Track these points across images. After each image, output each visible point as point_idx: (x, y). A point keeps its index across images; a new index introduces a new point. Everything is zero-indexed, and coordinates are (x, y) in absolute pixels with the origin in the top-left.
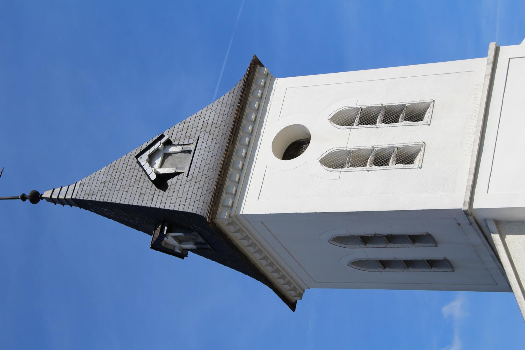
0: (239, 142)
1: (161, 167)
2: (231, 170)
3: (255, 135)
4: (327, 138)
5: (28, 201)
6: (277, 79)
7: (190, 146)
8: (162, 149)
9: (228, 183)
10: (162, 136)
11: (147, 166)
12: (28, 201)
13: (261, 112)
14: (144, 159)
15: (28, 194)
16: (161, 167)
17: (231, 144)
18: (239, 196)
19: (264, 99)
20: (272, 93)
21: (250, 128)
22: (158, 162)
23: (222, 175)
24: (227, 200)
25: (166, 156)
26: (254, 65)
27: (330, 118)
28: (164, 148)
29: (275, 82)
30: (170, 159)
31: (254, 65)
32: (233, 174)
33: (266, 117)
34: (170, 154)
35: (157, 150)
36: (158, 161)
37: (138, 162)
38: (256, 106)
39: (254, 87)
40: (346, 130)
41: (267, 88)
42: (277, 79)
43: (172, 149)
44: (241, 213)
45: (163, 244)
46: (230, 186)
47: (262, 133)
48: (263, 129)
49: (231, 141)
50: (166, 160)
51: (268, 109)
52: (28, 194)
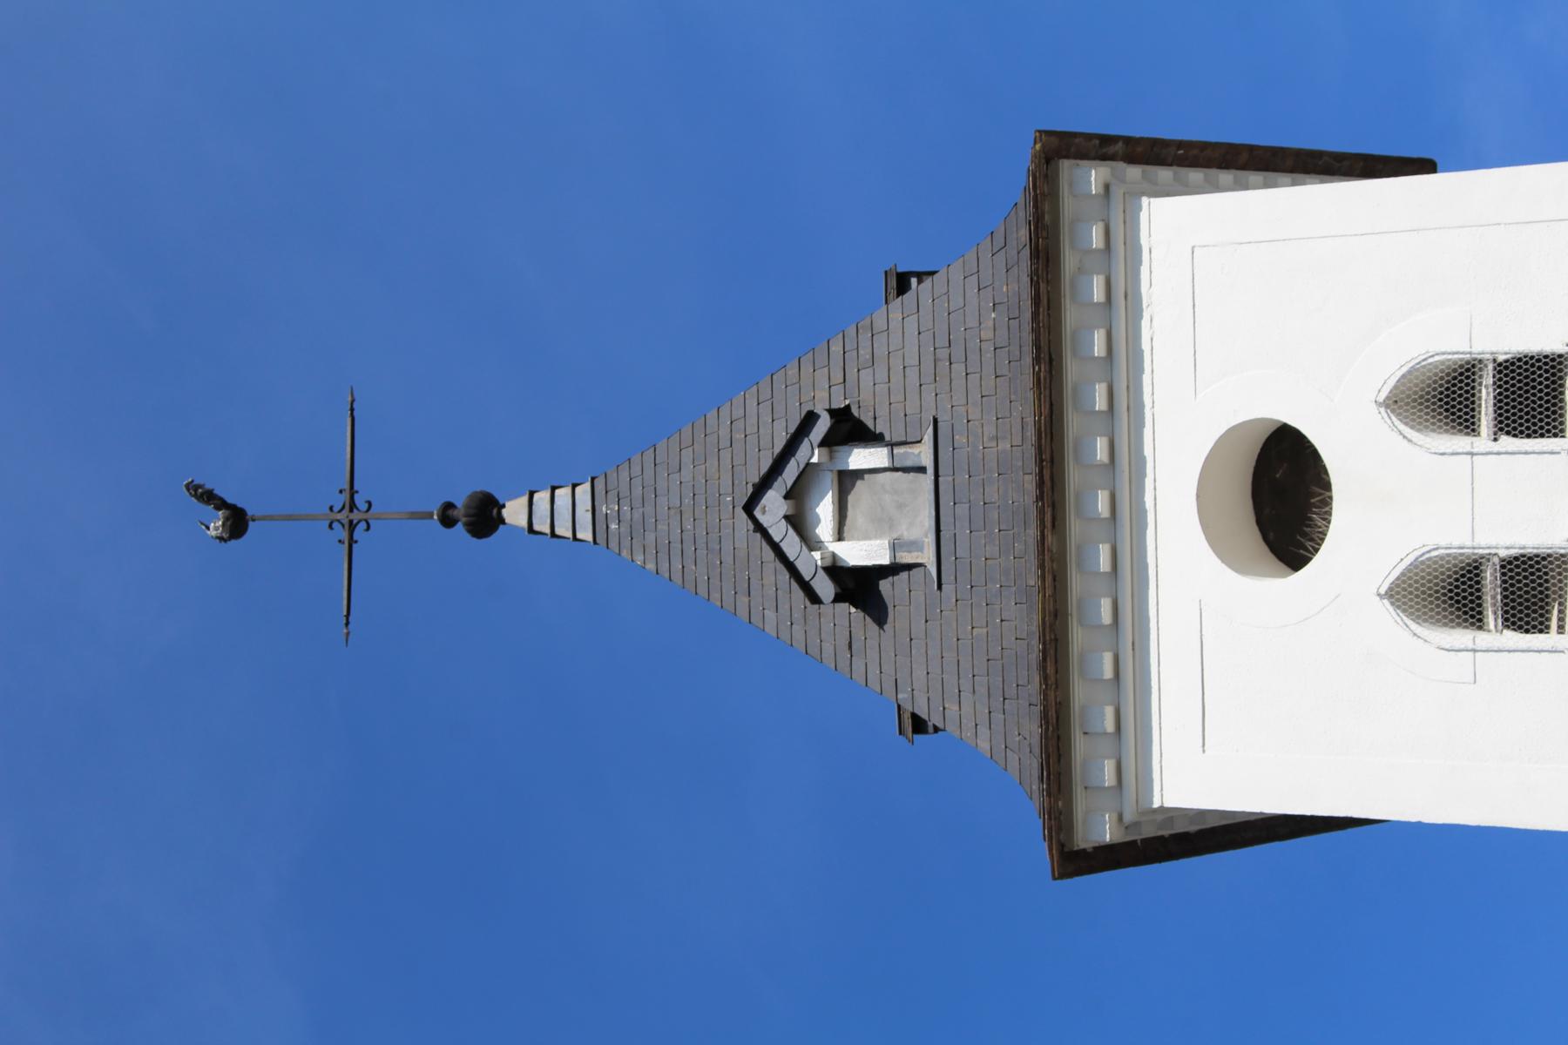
0: (1079, 565)
1: (840, 537)
2: (1080, 747)
3: (1124, 469)
4: (1405, 497)
5: (460, 528)
6: (1145, 200)
7: (915, 450)
8: (825, 459)
9: (1080, 693)
10: (810, 419)
11: (791, 545)
12: (460, 528)
13: (1125, 412)
14: (773, 508)
15: (460, 501)
16: (840, 537)
17: (1048, 532)
18: (1132, 736)
19: (1123, 305)
20: (1144, 270)
21: (1101, 445)
22: (825, 509)
23: (1052, 680)
24: (1095, 767)
25: (847, 480)
26: (1048, 161)
27: (1381, 398)
28: (831, 458)
29: (1143, 216)
30: (860, 495)
31: (1048, 161)
32: (1093, 661)
33: (1146, 378)
34: (859, 474)
35: (808, 470)
36: (825, 509)
37: (760, 528)
38: (1101, 454)
39: (1069, 261)
40: (1438, 455)
41: (1121, 254)
42: (1145, 200)
43: (861, 458)
44: (1156, 805)
45: (1065, 166)
46: (1093, 711)
47: (1148, 451)
48: (1147, 432)
49: (1048, 524)
50: (851, 498)
51: (1145, 346)
52: (460, 501)
